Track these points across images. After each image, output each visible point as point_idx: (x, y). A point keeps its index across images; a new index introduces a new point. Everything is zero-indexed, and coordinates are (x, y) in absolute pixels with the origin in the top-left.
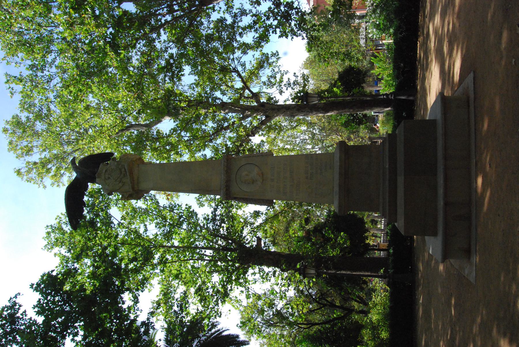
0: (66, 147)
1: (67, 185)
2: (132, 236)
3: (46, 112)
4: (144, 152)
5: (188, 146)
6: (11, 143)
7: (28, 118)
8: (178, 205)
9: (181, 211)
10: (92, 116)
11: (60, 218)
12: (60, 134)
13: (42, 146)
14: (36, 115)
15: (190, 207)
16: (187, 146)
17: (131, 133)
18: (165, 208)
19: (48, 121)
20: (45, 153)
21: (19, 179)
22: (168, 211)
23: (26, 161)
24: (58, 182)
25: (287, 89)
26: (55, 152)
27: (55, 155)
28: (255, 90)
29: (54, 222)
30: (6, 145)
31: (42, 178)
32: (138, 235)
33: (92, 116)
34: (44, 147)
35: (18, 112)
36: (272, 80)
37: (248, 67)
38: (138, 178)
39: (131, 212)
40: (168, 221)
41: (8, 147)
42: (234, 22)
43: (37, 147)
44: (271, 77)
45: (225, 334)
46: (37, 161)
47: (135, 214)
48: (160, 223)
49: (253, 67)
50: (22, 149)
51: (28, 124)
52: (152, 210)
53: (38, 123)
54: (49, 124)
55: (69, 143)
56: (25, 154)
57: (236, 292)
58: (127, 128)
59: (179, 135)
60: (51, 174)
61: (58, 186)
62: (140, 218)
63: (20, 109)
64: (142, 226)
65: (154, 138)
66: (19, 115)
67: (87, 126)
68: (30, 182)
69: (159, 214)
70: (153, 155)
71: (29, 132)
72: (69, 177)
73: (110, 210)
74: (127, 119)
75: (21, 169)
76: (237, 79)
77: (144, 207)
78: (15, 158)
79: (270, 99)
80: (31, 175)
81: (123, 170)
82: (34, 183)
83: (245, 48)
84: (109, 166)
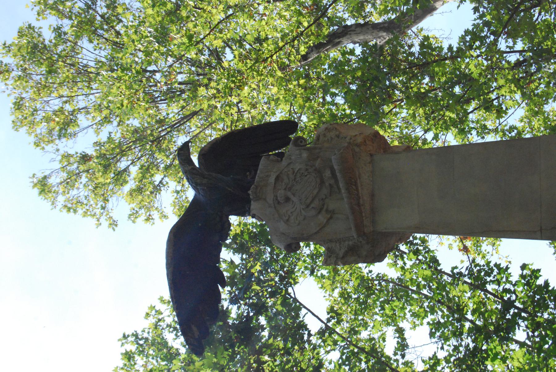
0: (163, 106)
1: (173, 220)
2: (363, 365)
3: (105, 10)
4: (386, 108)
5: (522, 84)
6: (18, 105)
7: (58, 30)
8: (497, 266)
9: (508, 286)
10: (230, 12)
11: (159, 312)
12: (145, 71)
13: (99, 108)
14: (80, 22)
15: (535, 274)
16: (516, 81)
17: (344, 54)
18: (456, 276)
19: (110, 35)
20: (107, 129)
21: (44, 204)
22: (466, 287)
23: (62, 152)
24: (148, 209)
26: (135, 123)
27: (136, 131)
29: (143, 326)
30: (8, 111)
31: (106, 200)
32: (379, 362)
33: (230, 12)
34: (105, 112)
35: (31, 17)
38: (372, 196)
39: (356, 290)
40: (469, 316)
41: (13, 118)
43: (88, 113)
46: (91, 151)
47: (368, 296)
48: (445, 325)
50: (48, 120)
51: (60, 48)
52: (418, 286)
53: (84, 43)
54: (115, 43)
55: (171, 95)
56: (56, 133)
58: (334, 39)
59: (492, 48)
60: (127, 188)
61: (148, 219)
62: (383, 308)
63: (37, 8)
64: (390, 331)
65: (416, 65)
66: (35, 24)
67: (218, 43)
68: (75, 211)
69: (439, 294)
70: (414, 116)
71: (64, 72)
72: (174, 196)
73: (296, 287)
74: (330, 11)
75: (49, 176)
77: (393, 274)
78: (32, 146)
80: (74, 192)
81: (328, 173)
82: (85, 214)
84: (284, 162)
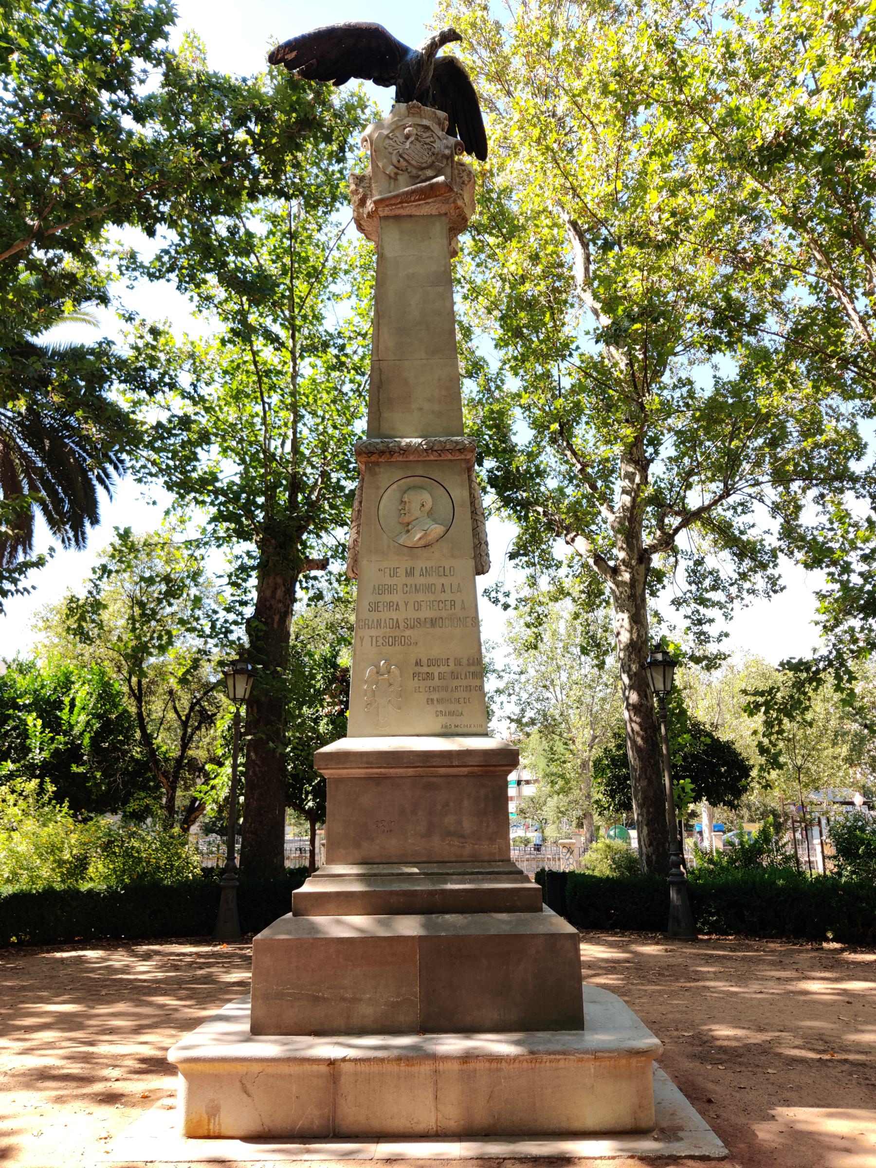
25: (686, 617)
28: (682, 540)
36: (707, 583)
37: (739, 522)
42: (854, 479)
44: (717, 579)
45: (100, 490)
49: (742, 533)
57: (199, 516)
76: (708, 499)
79: (659, 576)
81: (430, 173)
83: (788, 510)
